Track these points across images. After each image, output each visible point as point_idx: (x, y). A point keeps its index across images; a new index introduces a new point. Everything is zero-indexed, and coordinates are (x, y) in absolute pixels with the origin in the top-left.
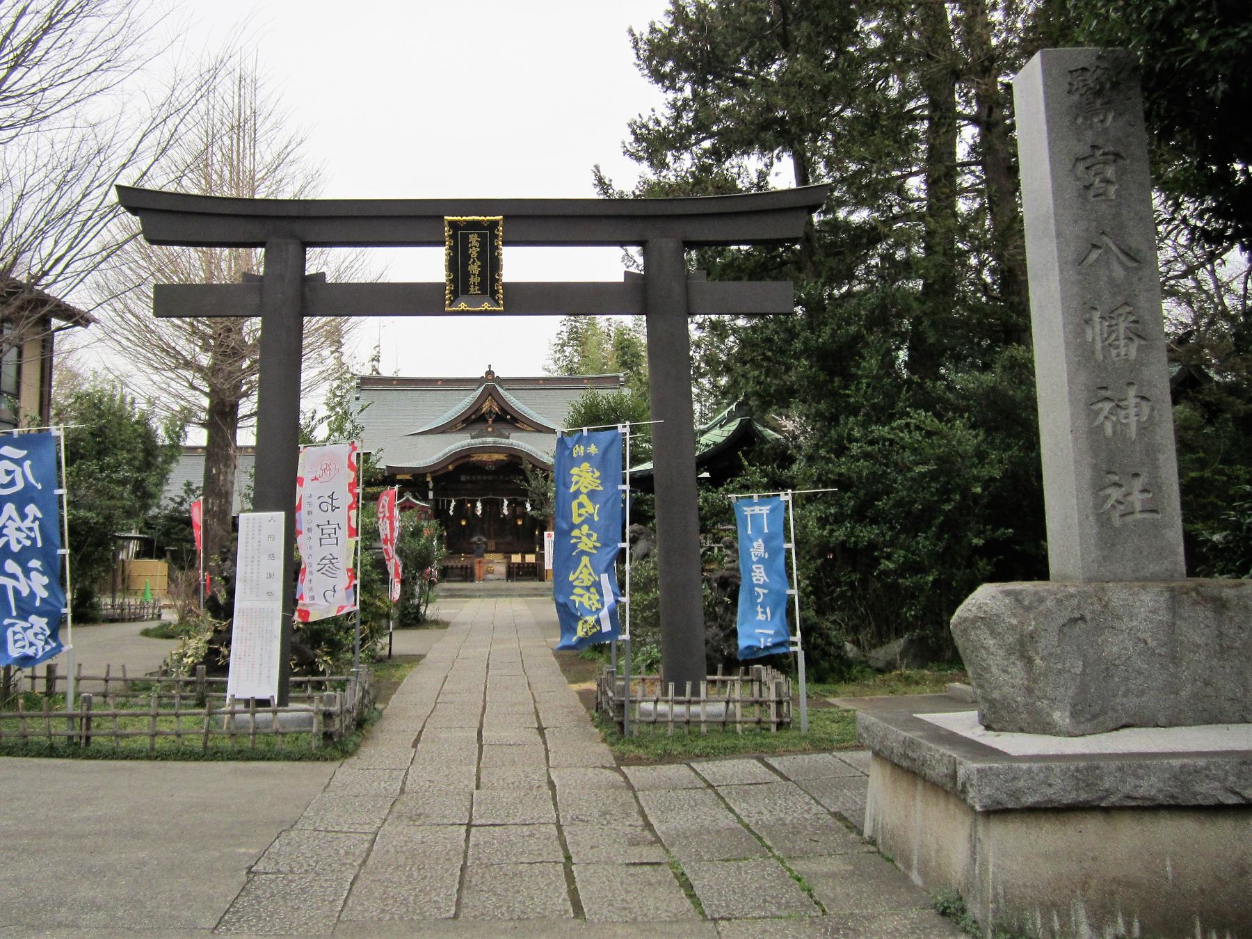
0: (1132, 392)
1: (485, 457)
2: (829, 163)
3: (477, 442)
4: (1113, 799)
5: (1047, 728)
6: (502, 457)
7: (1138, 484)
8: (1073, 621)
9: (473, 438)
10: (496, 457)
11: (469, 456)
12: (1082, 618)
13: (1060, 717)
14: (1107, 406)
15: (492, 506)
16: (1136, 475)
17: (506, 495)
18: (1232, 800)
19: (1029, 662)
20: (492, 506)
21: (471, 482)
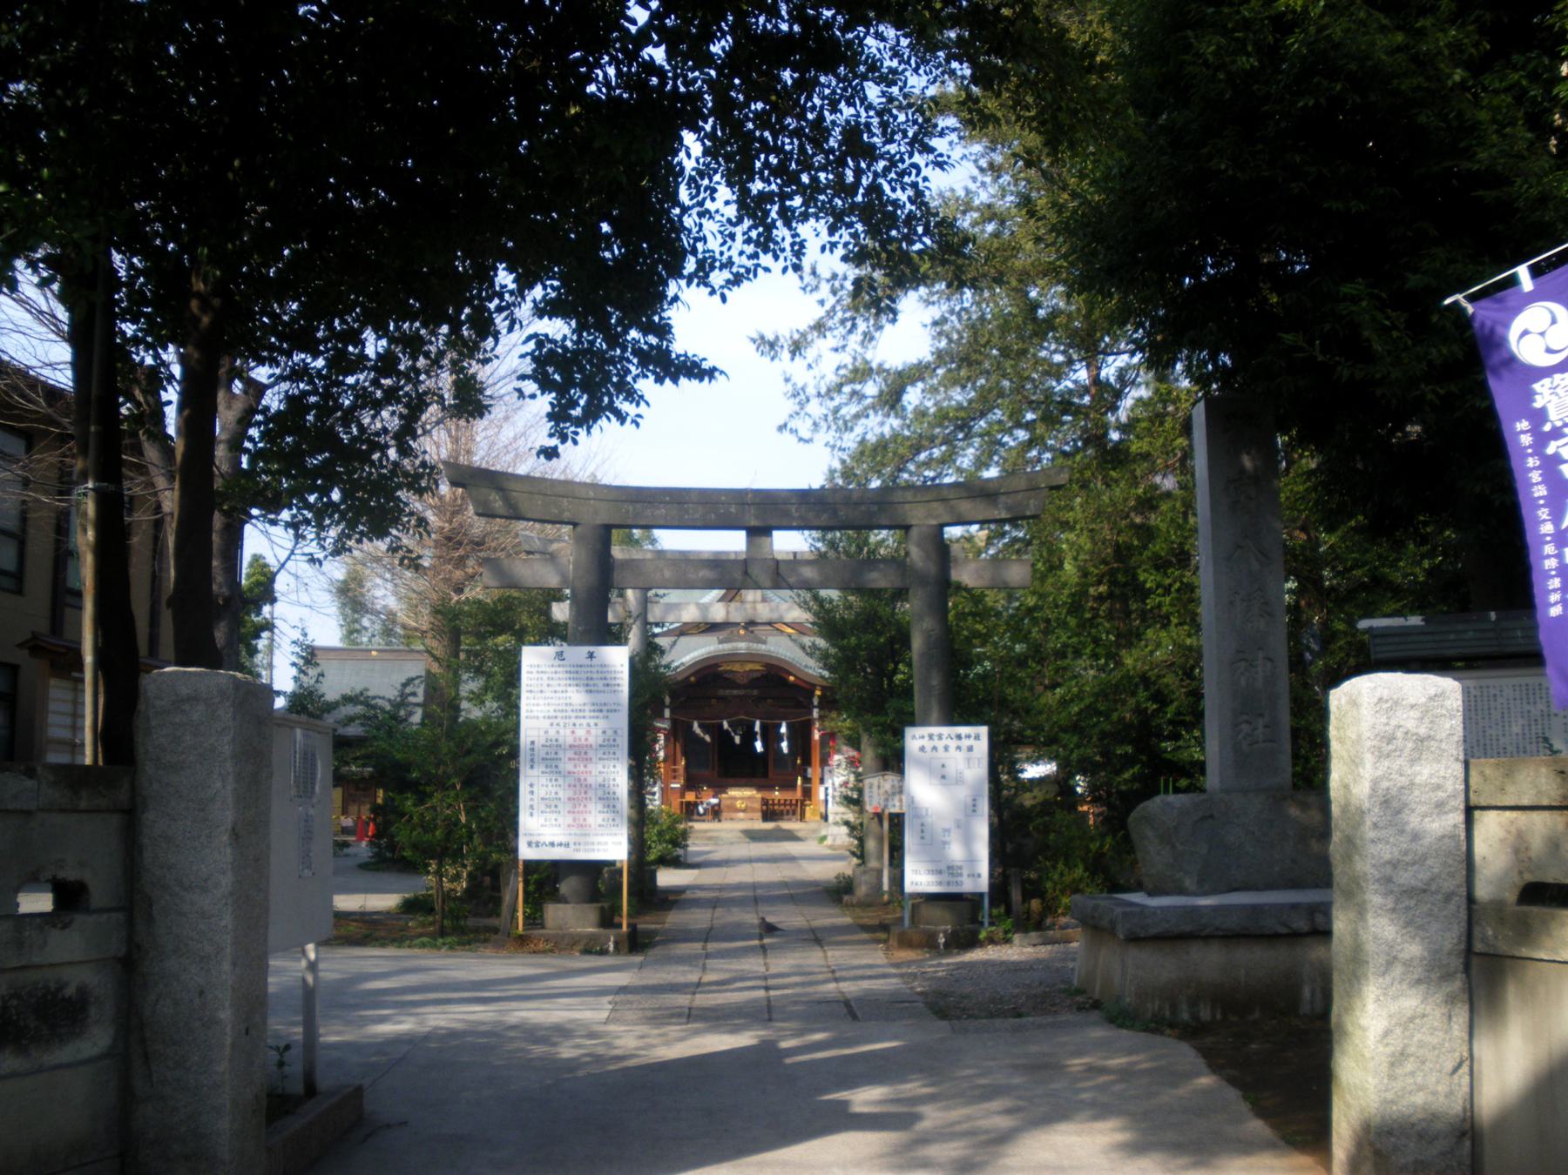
0: (1261, 654)
1: (737, 668)
2: (1456, 47)
3: (726, 648)
4: (1207, 931)
5: (1182, 891)
6: (758, 667)
7: (1261, 722)
8: (1204, 818)
9: (721, 642)
10: (749, 667)
11: (717, 665)
12: (1211, 817)
13: (1188, 883)
14: (1243, 664)
15: (330, 326)
16: (1261, 715)
17: (697, 718)
18: (1284, 931)
19: (1173, 847)
20: (330, 326)
21: (1092, 1070)
